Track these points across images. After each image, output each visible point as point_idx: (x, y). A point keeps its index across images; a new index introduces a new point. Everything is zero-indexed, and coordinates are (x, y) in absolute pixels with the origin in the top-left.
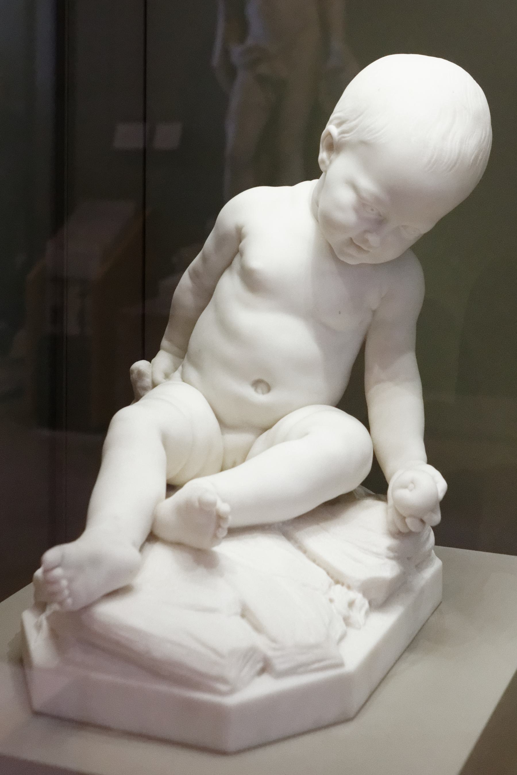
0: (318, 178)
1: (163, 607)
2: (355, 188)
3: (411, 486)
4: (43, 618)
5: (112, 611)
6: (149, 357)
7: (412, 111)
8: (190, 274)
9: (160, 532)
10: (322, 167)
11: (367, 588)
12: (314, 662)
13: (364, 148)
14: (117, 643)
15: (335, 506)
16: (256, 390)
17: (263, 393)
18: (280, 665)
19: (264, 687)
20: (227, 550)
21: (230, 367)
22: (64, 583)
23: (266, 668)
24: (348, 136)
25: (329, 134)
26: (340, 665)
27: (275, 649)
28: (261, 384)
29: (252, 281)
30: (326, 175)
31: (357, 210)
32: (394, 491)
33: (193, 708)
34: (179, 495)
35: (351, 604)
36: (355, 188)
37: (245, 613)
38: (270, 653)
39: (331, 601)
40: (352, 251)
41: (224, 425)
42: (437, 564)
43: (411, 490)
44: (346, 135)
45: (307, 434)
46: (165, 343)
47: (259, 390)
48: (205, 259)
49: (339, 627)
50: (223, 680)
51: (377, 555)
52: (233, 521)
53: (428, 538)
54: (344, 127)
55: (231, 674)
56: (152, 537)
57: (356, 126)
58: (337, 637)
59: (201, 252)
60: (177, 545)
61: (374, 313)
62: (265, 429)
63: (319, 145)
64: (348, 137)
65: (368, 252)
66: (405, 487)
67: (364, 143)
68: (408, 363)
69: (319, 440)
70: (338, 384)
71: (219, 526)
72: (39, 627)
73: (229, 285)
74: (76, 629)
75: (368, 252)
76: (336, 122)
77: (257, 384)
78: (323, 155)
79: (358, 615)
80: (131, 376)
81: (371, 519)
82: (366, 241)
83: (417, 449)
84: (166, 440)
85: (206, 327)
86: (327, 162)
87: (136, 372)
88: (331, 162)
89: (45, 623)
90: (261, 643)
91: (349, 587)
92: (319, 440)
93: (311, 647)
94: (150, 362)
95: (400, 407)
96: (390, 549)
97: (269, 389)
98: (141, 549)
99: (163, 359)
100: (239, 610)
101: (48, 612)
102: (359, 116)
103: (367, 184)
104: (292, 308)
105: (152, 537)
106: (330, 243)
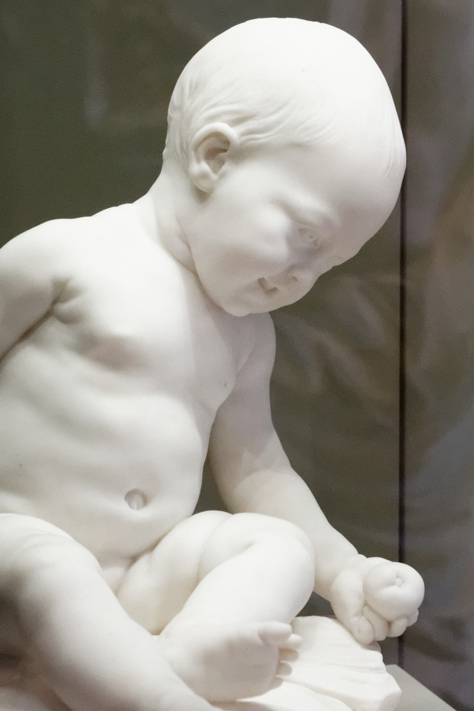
2: (289, 210)
3: (398, 581)
16: (130, 504)
17: (138, 508)
21: (97, 478)
24: (266, 137)
28: (139, 497)
31: (290, 240)
36: (289, 210)
43: (400, 586)
44: (257, 136)
45: (249, 546)
47: (135, 505)
51: (376, 670)
54: (250, 125)
57: (278, 123)
64: (262, 138)
66: (392, 584)
67: (299, 146)
77: (129, 496)
97: (145, 500)
102: (280, 108)
103: (310, 203)
104: (167, 386)
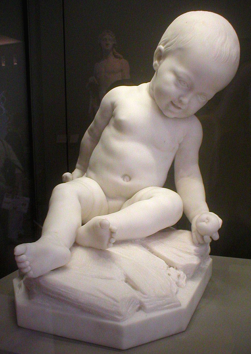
0: (150, 82)
1: (83, 276)
2: (175, 73)
4: (22, 281)
5: (58, 279)
6: (71, 171)
7: (203, 33)
8: (88, 131)
9: (79, 241)
10: (155, 68)
11: (186, 269)
12: (165, 305)
13: (181, 52)
14: (59, 294)
15: (165, 233)
16: (124, 179)
17: (127, 181)
18: (148, 306)
19: (140, 317)
20: (115, 250)
22: (27, 263)
23: (141, 307)
25: (160, 50)
26: (180, 305)
27: (145, 298)
29: (120, 127)
30: (157, 72)
32: (194, 226)
33: (100, 326)
34: (89, 224)
35: (179, 276)
36: (175, 73)
37: (128, 280)
38: (143, 300)
39: (169, 275)
40: (172, 108)
41: (108, 196)
42: (211, 260)
43: (206, 223)
46: (78, 165)
48: (95, 124)
49: (175, 288)
50: (119, 314)
51: (190, 253)
52: (118, 236)
53: (208, 249)
55: (123, 310)
56: (76, 244)
57: (175, 41)
58: (175, 292)
59: (94, 120)
60: (89, 248)
61: (180, 145)
62: (129, 198)
63: (153, 58)
64: (170, 48)
65: (180, 108)
67: (181, 49)
68: (195, 169)
69: (155, 203)
70: (163, 177)
71: (111, 237)
72: (20, 286)
73: (109, 132)
74: (34, 286)
75: (180, 108)
76: (162, 43)
78: (155, 62)
79: (183, 281)
80: (63, 180)
81: (184, 237)
82: (180, 102)
83: (204, 206)
84: (80, 199)
85: (98, 153)
86: (158, 65)
87: (65, 177)
88: (160, 64)
89: (23, 285)
90: (136, 294)
91: (176, 269)
92: (155, 203)
93: (164, 297)
94: (71, 173)
95: (194, 188)
96: (195, 250)
97: (130, 179)
98: (71, 249)
99: (77, 172)
100: (124, 279)
101: (24, 279)
102: (176, 36)
105: (76, 244)
106: (160, 107)
